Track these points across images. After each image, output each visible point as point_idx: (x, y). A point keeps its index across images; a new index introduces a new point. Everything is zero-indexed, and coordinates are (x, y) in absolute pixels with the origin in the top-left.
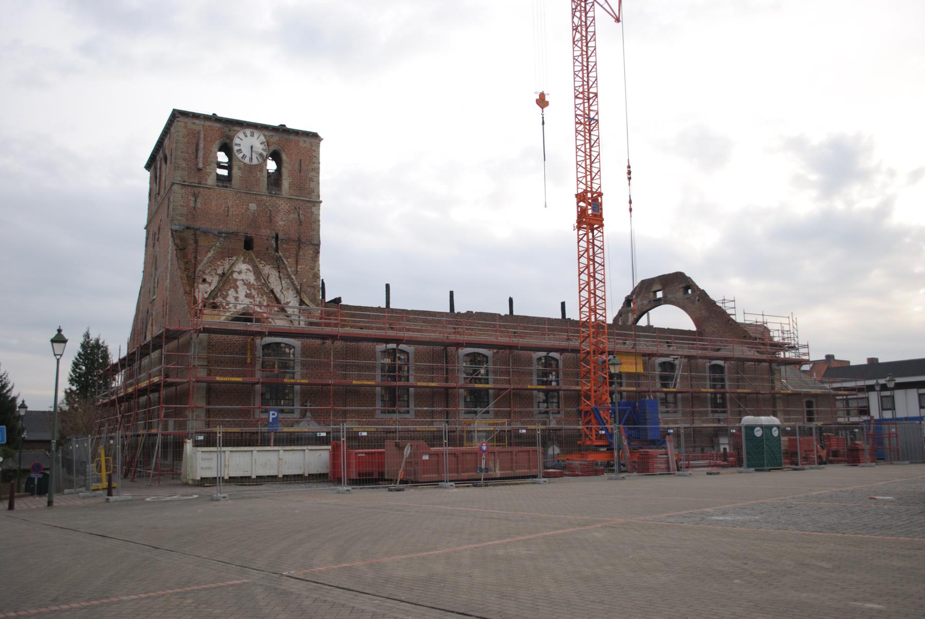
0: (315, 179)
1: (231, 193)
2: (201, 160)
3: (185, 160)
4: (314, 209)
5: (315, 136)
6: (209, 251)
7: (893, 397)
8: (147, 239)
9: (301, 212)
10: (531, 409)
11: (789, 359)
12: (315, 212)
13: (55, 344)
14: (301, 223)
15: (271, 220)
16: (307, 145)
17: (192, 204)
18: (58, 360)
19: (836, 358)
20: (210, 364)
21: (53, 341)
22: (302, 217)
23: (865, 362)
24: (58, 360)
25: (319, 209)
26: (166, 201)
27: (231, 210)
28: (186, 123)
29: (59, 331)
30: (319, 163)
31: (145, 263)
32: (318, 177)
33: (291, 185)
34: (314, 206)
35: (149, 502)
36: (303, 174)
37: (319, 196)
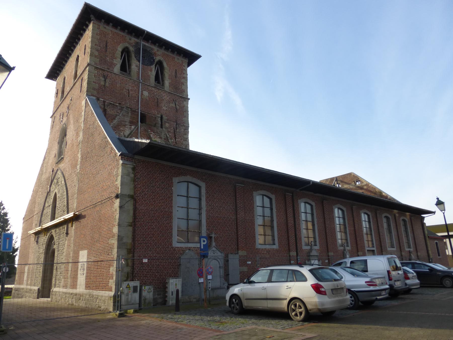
0: (185, 84)
3: (98, 50)
4: (185, 103)
6: (115, 119)
7: (366, 261)
9: (177, 103)
10: (213, 237)
11: (299, 216)
14: (177, 110)
17: (103, 83)
18: (444, 213)
22: (177, 107)
24: (444, 213)
25: (188, 104)
27: (131, 92)
29: (438, 199)
30: (187, 75)
32: (187, 83)
33: (170, 84)
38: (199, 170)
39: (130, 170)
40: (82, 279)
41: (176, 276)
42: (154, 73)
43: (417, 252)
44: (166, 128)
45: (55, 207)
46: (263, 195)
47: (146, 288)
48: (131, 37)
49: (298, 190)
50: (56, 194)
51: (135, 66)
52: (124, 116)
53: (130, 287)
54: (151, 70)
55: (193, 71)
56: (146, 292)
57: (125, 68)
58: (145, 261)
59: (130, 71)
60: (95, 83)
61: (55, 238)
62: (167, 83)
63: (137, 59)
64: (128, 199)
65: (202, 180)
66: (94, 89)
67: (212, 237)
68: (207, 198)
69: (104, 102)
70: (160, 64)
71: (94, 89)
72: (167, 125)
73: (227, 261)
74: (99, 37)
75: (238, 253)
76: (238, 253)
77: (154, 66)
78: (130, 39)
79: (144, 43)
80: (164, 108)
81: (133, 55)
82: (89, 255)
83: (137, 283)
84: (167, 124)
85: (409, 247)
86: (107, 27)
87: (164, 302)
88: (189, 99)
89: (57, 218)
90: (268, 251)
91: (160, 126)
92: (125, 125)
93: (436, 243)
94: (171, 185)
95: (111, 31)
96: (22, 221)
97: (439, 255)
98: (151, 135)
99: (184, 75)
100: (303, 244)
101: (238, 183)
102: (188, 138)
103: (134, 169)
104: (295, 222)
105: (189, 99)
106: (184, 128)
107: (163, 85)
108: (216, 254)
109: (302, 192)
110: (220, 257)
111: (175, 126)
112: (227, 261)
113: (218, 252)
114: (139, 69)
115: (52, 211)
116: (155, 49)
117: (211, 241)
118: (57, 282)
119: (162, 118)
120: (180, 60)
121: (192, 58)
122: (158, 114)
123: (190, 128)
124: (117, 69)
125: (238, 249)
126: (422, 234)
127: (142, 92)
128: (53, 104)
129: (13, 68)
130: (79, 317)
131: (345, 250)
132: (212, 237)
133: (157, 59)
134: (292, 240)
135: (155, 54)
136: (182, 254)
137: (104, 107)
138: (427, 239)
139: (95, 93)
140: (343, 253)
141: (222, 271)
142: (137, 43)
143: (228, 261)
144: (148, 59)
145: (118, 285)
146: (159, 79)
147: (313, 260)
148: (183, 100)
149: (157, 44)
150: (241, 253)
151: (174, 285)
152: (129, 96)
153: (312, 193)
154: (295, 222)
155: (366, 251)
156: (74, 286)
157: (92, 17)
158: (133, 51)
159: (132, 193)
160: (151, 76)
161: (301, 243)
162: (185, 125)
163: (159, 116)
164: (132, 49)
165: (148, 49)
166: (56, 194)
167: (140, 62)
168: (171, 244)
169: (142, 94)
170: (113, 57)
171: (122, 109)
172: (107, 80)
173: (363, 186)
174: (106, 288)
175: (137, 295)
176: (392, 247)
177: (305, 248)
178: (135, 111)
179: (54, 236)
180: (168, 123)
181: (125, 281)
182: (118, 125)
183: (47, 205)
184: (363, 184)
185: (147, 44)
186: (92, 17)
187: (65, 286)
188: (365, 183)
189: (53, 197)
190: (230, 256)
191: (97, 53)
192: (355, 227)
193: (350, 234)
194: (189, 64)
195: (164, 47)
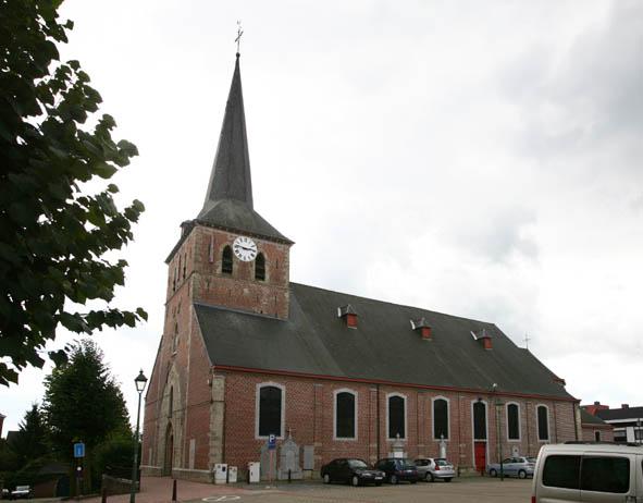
2: (212, 257)
5: (290, 243)
7: (625, 431)
8: (167, 316)
13: (139, 383)
16: (281, 249)
17: (206, 287)
19: (304, 269)
21: (137, 380)
23: (620, 407)
26: (186, 285)
31: (165, 328)
35: (188, 445)
40: (192, 462)
55: (292, 249)
62: (267, 276)
73: (302, 450)
82: (196, 442)
83: (226, 465)
87: (247, 481)
112: (302, 450)
130: (136, 456)
141: (297, 458)
150: (316, 444)
151: (255, 468)
156: (187, 467)
172: (211, 285)
187: (181, 467)
190: (306, 448)
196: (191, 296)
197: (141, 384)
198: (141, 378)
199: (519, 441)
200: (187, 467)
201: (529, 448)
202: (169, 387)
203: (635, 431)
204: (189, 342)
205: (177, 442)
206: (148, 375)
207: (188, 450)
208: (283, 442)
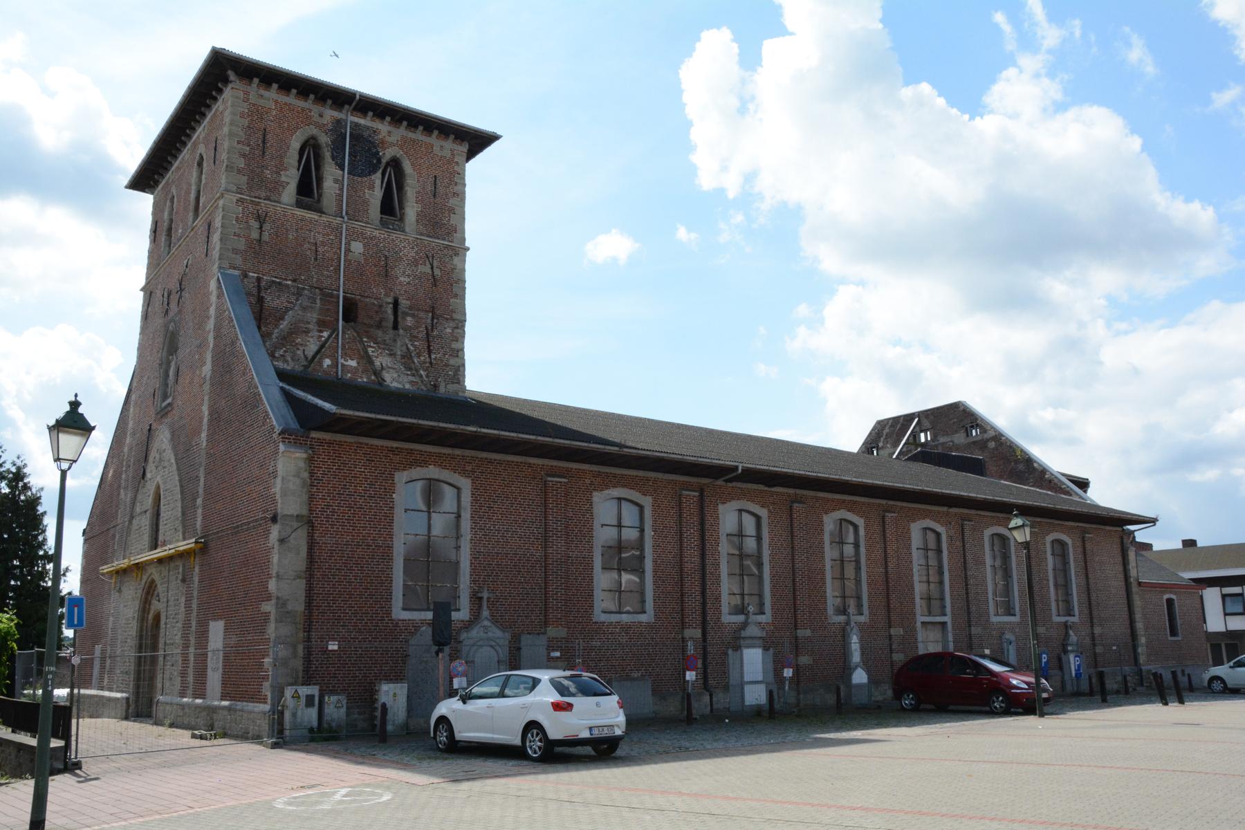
1: (304, 201)
3: (244, 156)
4: (456, 260)
6: (282, 318)
9: (435, 264)
12: (459, 266)
15: (386, 273)
18: (64, 474)
20: (945, 615)
24: (64, 474)
28: (246, 93)
30: (464, 185)
34: (457, 254)
35: (203, 635)
36: (438, 200)
37: (464, 239)
38: (458, 452)
39: (302, 464)
40: (214, 679)
41: (396, 678)
42: (378, 193)
43: (1092, 626)
44: (407, 329)
45: (158, 514)
46: (620, 499)
47: (331, 700)
48: (322, 109)
49: (720, 482)
50: (158, 487)
51: (333, 179)
52: (304, 309)
53: (299, 697)
54: (372, 187)
55: (477, 170)
56: (332, 706)
57: (308, 189)
58: (333, 646)
59: (320, 195)
60: (239, 236)
61: (161, 589)
62: (411, 212)
63: (336, 164)
64: (296, 525)
65: (464, 473)
66: (235, 251)
67: (481, 598)
68: (474, 513)
69: (259, 279)
70: (395, 163)
71: (235, 251)
72: (409, 321)
74: (246, 122)
75: (545, 633)
76: (545, 633)
77: (379, 174)
78: (321, 116)
79: (356, 120)
80: (402, 279)
81: (327, 155)
82: (227, 630)
83: (314, 690)
84: (409, 319)
85: (1069, 613)
86: (266, 94)
88: (468, 249)
89: (164, 544)
90: (626, 628)
91: (390, 324)
92: (307, 332)
93: (1170, 601)
94: (390, 490)
95: (276, 102)
96: (81, 539)
97: (1174, 632)
98: (370, 350)
99: (456, 189)
100: (725, 609)
101: (553, 476)
102: (462, 350)
103: (310, 460)
104: (703, 556)
105: (468, 249)
106: (452, 324)
107: (402, 219)
108: (490, 634)
109: (730, 484)
110: (501, 642)
111: (429, 321)
113: (494, 629)
114: (341, 189)
115: (151, 525)
116: (383, 128)
117: (480, 607)
118: (167, 684)
119: (396, 303)
120: (446, 147)
121: (477, 141)
122: (387, 295)
123: (467, 324)
124: (289, 193)
125: (546, 624)
126: (1121, 576)
127: (348, 244)
128: (146, 254)
129: (94, 428)
131: (848, 623)
132: (481, 598)
133: (388, 154)
134: (693, 602)
135: (383, 142)
136: (412, 634)
137: (259, 291)
138: (1135, 589)
139: (238, 260)
140: (844, 630)
142: (338, 122)
143: (519, 649)
144: (364, 157)
145: (279, 692)
146: (390, 207)
147: (748, 647)
148: (451, 252)
149: (388, 119)
150: (552, 631)
152: (316, 259)
153: (762, 487)
154: (703, 556)
155: (919, 624)
156: (200, 692)
157: (232, 75)
158: (327, 145)
159: (305, 512)
160: (372, 201)
161: (718, 609)
162: (455, 316)
163: (390, 300)
164: (324, 139)
165: (366, 134)
166: (158, 487)
167: (343, 170)
168: (389, 613)
169: (348, 250)
170: (280, 168)
171: (299, 294)
172: (267, 226)
173: (988, 440)
174: (257, 697)
175: (313, 713)
176: (1009, 611)
177: (728, 618)
178: (331, 296)
179: (158, 582)
180: (413, 316)
181: (292, 684)
182: (291, 333)
183: (138, 510)
184: (986, 436)
185: (362, 121)
186: (232, 75)
188: (992, 433)
189: (152, 492)
190: (526, 640)
191: (241, 163)
192: (886, 567)
193: (869, 584)
194: (471, 154)
195: (405, 123)
196: (216, 253)
197: (69, 441)
198: (73, 422)
199: (1075, 619)
200: (200, 692)
201: (890, 636)
202: (150, 488)
203: (1224, 596)
204: (207, 369)
205: (171, 633)
206: (104, 417)
207: (202, 660)
208: (468, 625)
